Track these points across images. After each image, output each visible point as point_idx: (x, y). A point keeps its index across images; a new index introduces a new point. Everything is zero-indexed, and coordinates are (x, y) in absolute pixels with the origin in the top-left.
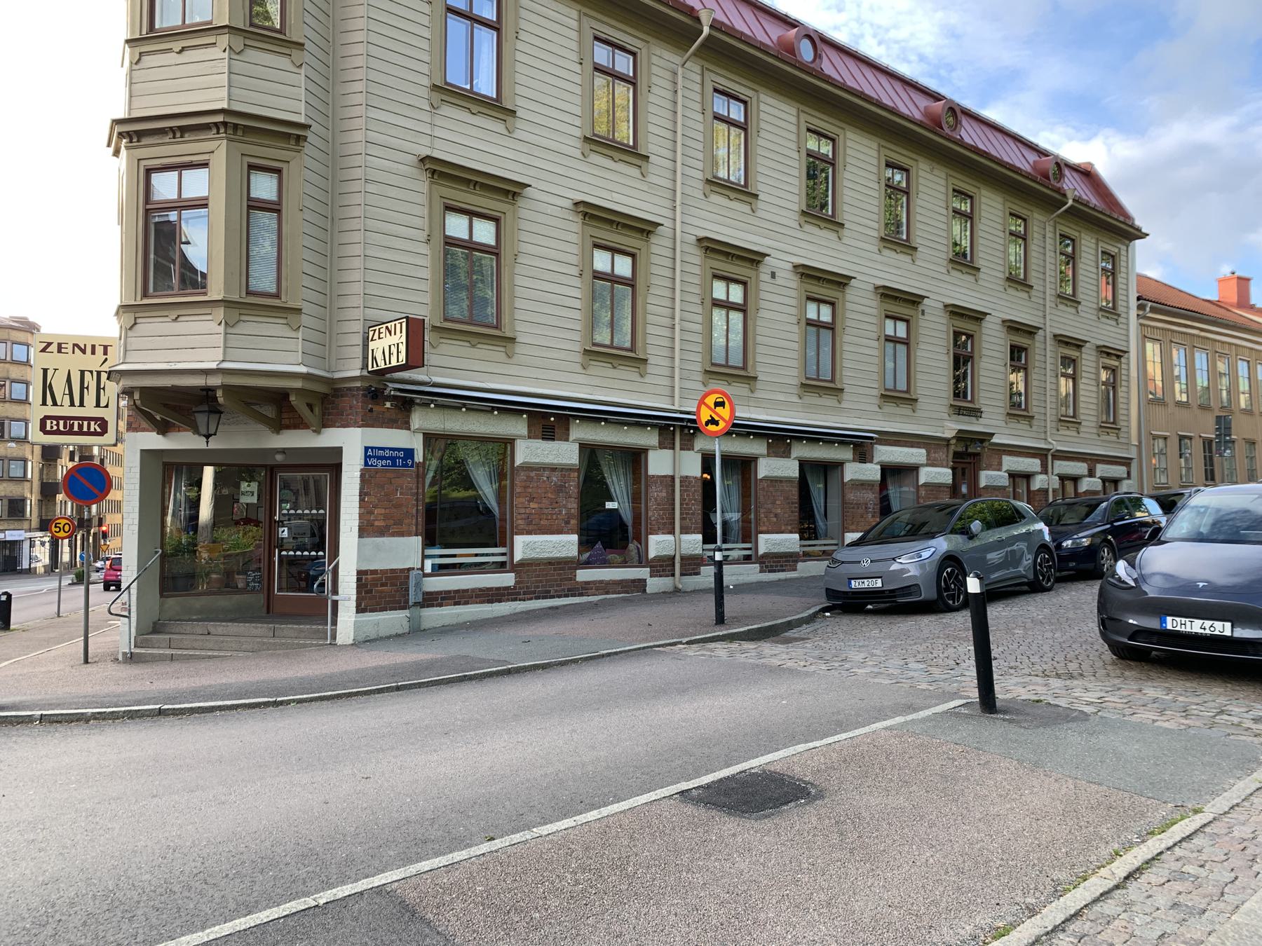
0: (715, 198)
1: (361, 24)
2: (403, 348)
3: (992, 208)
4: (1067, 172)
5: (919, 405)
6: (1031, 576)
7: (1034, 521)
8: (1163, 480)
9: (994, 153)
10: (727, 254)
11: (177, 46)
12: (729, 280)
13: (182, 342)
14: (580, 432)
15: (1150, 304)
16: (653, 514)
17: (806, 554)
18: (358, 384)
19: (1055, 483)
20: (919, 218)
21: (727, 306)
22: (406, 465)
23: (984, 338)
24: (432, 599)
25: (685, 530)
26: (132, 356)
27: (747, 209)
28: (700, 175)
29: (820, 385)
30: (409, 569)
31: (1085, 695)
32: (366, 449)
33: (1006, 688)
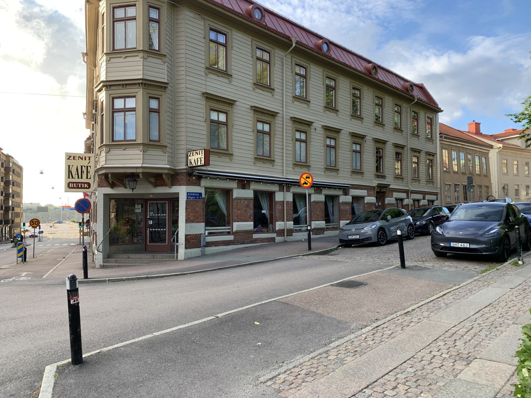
0: (296, 103)
1: (183, 47)
2: (203, 159)
3: (389, 102)
4: (414, 87)
5: (364, 175)
6: (407, 234)
7: (407, 216)
8: (449, 201)
9: (390, 83)
10: (300, 122)
11: (124, 56)
12: (301, 132)
13: (126, 157)
14: (254, 186)
15: (444, 136)
16: (277, 214)
17: (327, 228)
18: (185, 171)
19: (411, 202)
20: (364, 107)
21: (300, 141)
22: (199, 198)
23: (387, 150)
24: (209, 244)
25: (288, 220)
26: (108, 162)
28: (291, 95)
29: (332, 168)
30: (201, 234)
31: (429, 265)
32: (187, 193)
33: (407, 264)
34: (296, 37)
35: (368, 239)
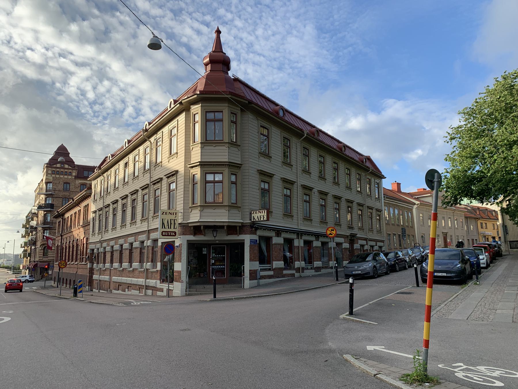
11: (214, 145)
14: (284, 235)
27: (309, 176)
34: (306, 130)
35: (366, 274)
